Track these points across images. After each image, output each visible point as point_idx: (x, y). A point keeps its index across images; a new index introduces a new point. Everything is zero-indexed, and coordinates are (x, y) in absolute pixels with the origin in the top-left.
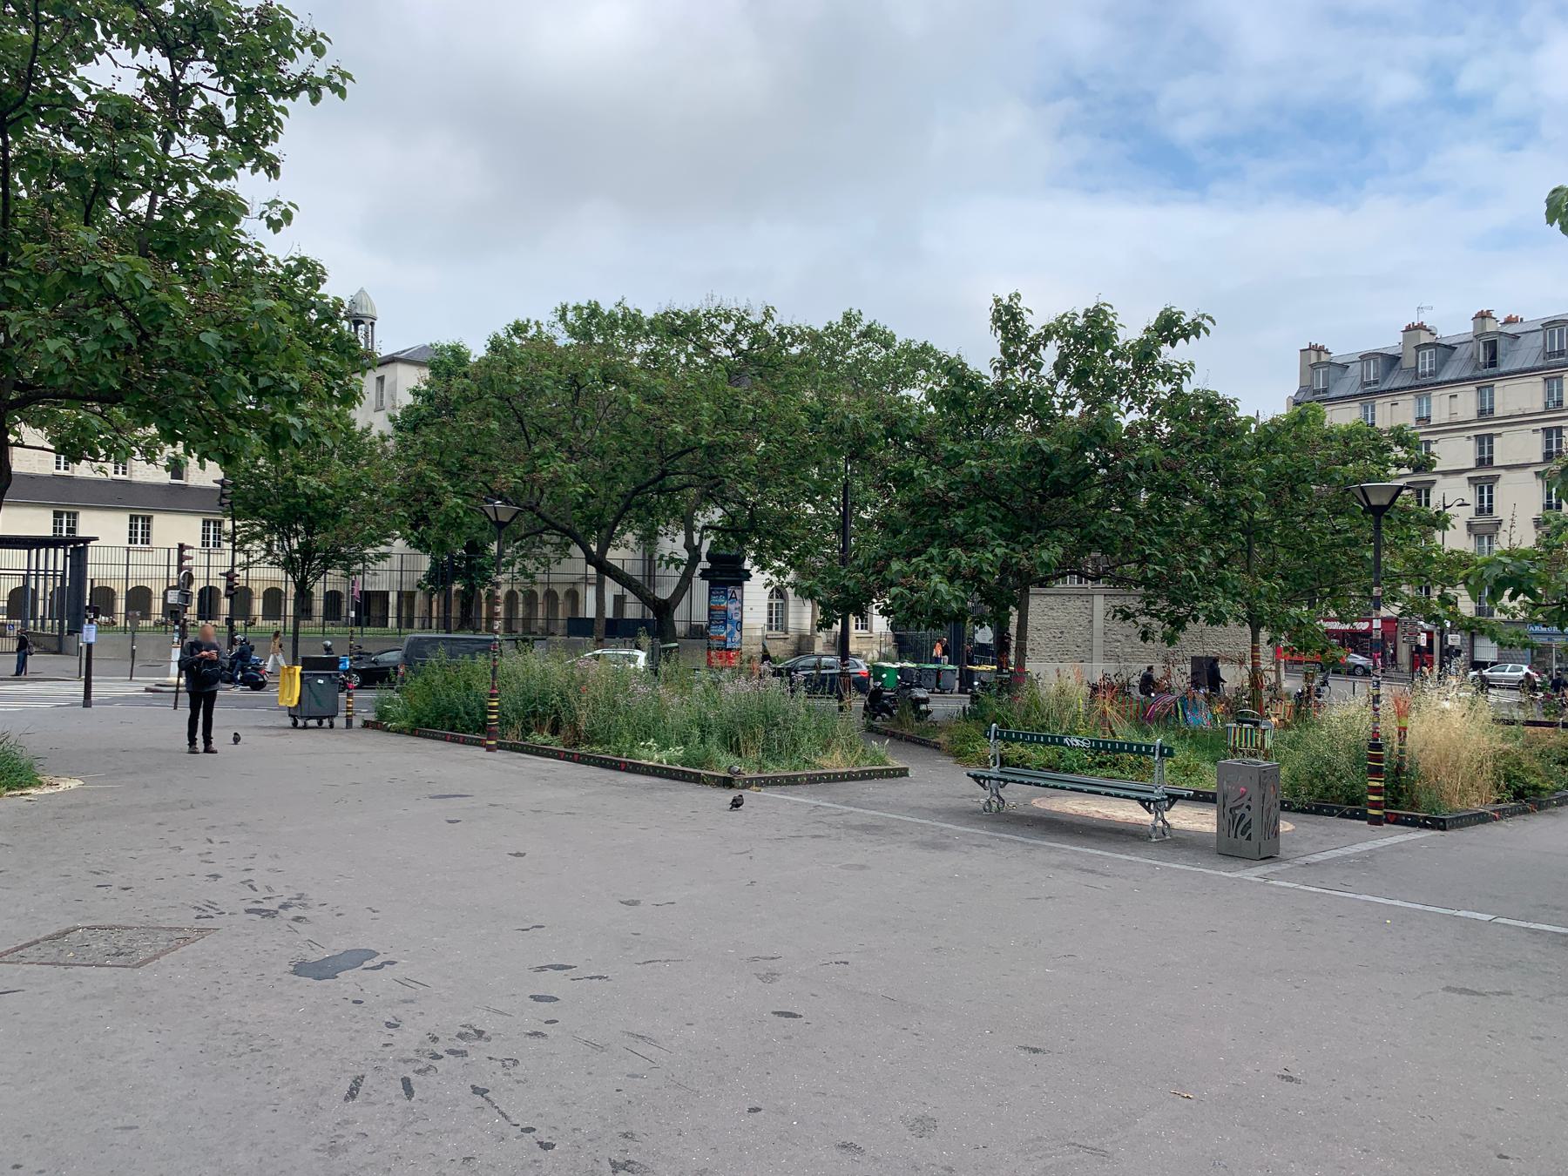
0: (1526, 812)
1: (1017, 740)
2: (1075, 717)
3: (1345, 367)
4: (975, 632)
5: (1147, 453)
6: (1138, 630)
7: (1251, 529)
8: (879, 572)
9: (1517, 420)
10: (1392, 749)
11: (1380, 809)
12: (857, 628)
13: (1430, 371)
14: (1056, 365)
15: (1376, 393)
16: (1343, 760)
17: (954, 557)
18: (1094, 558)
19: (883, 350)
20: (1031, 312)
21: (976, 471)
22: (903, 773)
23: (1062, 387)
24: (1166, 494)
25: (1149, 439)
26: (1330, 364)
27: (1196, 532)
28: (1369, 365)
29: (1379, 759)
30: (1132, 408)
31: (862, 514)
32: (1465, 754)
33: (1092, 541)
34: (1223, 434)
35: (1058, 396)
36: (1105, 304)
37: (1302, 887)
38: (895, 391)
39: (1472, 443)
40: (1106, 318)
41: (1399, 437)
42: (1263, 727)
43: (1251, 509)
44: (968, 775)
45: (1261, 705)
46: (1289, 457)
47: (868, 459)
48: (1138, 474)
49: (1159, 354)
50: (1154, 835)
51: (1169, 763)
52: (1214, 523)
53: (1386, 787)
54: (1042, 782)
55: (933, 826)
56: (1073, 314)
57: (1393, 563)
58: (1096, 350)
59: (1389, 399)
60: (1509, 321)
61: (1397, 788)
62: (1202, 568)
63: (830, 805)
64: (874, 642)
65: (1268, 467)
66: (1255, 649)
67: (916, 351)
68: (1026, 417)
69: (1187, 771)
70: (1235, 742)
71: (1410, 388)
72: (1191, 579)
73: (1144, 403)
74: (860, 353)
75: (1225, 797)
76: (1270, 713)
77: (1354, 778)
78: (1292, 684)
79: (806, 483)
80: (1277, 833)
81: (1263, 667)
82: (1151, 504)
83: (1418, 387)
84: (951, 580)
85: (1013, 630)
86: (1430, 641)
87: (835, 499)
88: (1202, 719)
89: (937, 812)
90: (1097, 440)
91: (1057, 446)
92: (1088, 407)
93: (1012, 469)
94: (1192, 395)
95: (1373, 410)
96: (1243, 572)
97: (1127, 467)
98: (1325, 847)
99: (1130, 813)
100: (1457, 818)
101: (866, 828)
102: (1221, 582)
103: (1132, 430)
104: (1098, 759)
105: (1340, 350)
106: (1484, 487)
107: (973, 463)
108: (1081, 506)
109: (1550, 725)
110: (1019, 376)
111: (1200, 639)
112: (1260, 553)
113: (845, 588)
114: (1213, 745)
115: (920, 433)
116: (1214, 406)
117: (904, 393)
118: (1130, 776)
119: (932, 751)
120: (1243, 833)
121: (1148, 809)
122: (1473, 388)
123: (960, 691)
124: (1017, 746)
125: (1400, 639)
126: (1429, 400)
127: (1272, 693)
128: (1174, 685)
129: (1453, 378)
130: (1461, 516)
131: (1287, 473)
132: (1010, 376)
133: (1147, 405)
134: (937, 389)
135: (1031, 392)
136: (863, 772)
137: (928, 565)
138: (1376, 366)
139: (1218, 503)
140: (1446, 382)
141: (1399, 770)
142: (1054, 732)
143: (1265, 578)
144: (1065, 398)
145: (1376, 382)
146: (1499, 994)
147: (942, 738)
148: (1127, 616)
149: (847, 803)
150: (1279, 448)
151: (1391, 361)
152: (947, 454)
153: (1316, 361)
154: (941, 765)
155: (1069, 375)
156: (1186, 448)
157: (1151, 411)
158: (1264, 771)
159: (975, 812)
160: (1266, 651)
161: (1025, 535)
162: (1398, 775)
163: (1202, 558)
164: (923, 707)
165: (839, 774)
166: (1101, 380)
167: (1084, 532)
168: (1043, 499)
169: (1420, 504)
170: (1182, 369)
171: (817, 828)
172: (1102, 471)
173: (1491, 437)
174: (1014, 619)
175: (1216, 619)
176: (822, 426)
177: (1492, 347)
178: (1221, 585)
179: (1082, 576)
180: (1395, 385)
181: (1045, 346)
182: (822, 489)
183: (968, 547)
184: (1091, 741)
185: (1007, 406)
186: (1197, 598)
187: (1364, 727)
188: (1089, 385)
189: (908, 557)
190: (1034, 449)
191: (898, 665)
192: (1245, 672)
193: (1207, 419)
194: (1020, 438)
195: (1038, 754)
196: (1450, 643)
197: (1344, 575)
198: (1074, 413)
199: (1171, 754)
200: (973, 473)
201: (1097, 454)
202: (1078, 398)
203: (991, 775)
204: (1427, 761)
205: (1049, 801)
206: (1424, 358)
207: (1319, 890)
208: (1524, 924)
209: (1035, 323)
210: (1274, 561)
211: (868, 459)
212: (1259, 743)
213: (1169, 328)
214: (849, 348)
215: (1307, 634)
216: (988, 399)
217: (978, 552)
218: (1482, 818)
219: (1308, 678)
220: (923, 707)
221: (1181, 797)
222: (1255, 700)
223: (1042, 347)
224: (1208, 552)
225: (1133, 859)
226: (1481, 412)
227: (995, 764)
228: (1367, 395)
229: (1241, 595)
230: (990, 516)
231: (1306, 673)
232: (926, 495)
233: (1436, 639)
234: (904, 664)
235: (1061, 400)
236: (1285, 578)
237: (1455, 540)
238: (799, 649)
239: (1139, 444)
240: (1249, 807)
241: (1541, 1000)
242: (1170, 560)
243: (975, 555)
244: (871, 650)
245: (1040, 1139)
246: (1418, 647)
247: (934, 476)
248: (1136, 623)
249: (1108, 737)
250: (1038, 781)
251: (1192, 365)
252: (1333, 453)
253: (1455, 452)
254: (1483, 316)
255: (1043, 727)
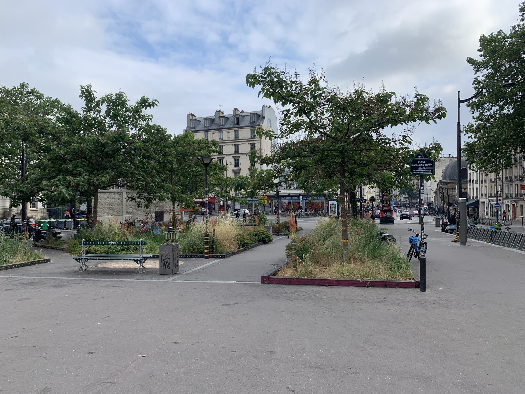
0: (245, 250)
1: (92, 244)
2: (115, 234)
3: (200, 121)
4: (80, 207)
5: (138, 144)
6: (136, 204)
7: (172, 170)
8: (37, 185)
9: (244, 140)
10: (211, 236)
11: (208, 254)
12: (31, 207)
13: (223, 125)
14: (106, 112)
15: (208, 130)
16: (198, 241)
17: (68, 179)
18: (120, 180)
19: (39, 100)
20: (96, 92)
21: (76, 148)
22: (48, 261)
23: (108, 120)
24: (145, 158)
25: (139, 140)
26: (195, 120)
27: (154, 171)
28: (206, 121)
29: (207, 239)
30: (133, 129)
31: (31, 163)
32: (230, 236)
33: (120, 174)
34: (162, 140)
35: (107, 123)
36: (123, 92)
37: (185, 281)
38: (44, 116)
39: (233, 146)
40: (123, 97)
41: (213, 143)
42: (176, 232)
43: (172, 164)
44: (73, 259)
45: (176, 226)
46: (183, 148)
47: (33, 141)
48: (135, 151)
49: (141, 111)
50: (139, 271)
51: (145, 247)
52: (160, 168)
53: (210, 247)
54: (101, 258)
55: (59, 279)
56: (112, 94)
57: (211, 180)
58: (120, 108)
59: (212, 132)
60: (242, 112)
61: (213, 247)
62: (156, 183)
63: (15, 277)
64: (38, 212)
65: (176, 151)
66: (174, 208)
67: (53, 101)
68: (95, 130)
69: (151, 249)
70: (167, 238)
71: (217, 129)
72: (153, 187)
73: (137, 127)
74: (28, 100)
75: (162, 256)
76: (179, 228)
77: (201, 246)
78: (186, 219)
79: (4, 150)
80: (178, 265)
81: (176, 213)
82: (140, 162)
83: (219, 129)
84: (67, 187)
85: (93, 205)
86: (224, 204)
87: (19, 156)
88: (157, 232)
89: (60, 274)
90: (120, 140)
91: (106, 141)
92: (118, 127)
93: (90, 147)
94: (152, 126)
95: (208, 135)
96: (169, 184)
97: (131, 149)
98: (192, 268)
99: (132, 265)
100: (229, 254)
101: (30, 284)
102: (163, 187)
103: (133, 136)
104: (122, 248)
105: (199, 115)
106: (236, 159)
107: (75, 145)
108: (117, 161)
109: (251, 225)
110: (93, 115)
111: (156, 206)
112: (175, 178)
113: (22, 192)
114: (159, 239)
115: (54, 133)
116: (160, 130)
117: (48, 117)
118: (133, 253)
119: (62, 251)
120: (167, 267)
121: (137, 263)
122: (233, 130)
123: (74, 229)
124: (93, 246)
125: (216, 203)
126: (222, 133)
127: (179, 222)
128: (149, 221)
129: (228, 127)
130: (230, 168)
131: (182, 153)
132: (89, 114)
133: (138, 128)
134: (60, 117)
135: (97, 121)
136: (31, 263)
137: (58, 182)
138: (208, 121)
139: (161, 162)
140: (227, 128)
141: (213, 242)
142: (107, 240)
143: (176, 186)
144: (109, 123)
145: (208, 127)
146: (235, 304)
147: (65, 246)
148: (133, 199)
149: (23, 275)
150: (180, 145)
151: (212, 121)
152: (65, 141)
153: (191, 118)
154: (64, 256)
155: (111, 116)
156: (151, 144)
157: (139, 130)
158: (174, 246)
159: (76, 272)
160: (177, 209)
161: (96, 171)
162: (213, 243)
163: (156, 180)
164: (58, 235)
165: (20, 264)
166: (122, 118)
167: (118, 170)
168: (102, 159)
169: (220, 163)
170: (149, 117)
171: (8, 287)
172: (123, 150)
173: (238, 145)
174: (93, 201)
175: (161, 199)
176: (11, 127)
177: (238, 119)
178: (163, 188)
179: (119, 186)
180: (214, 128)
181: (102, 105)
182: (12, 152)
183: (74, 175)
184: (118, 242)
185: (88, 125)
186: (155, 192)
187: (203, 231)
188: (118, 120)
189: (50, 179)
190: (98, 141)
191: (49, 220)
192: (171, 216)
193: (157, 134)
194: (93, 137)
195: (101, 249)
196: (228, 204)
197: (199, 185)
198: (113, 129)
199: (145, 244)
200: (75, 149)
201: (121, 144)
202: (114, 124)
203: (82, 258)
204: (220, 238)
205: (104, 264)
206: (221, 121)
207: (190, 281)
208: (242, 283)
209: (98, 96)
210: (179, 181)
211: (33, 141)
212: (175, 238)
213: (144, 103)
214: (23, 97)
215: (189, 203)
216: (80, 122)
217: (78, 178)
218: (234, 254)
219: (190, 217)
220: (58, 235)
221: (148, 258)
222: (174, 225)
223: (100, 105)
224: (158, 177)
225: (132, 280)
226: (236, 138)
227: (84, 253)
228: (206, 130)
229: (169, 191)
230: (83, 164)
231: (189, 215)
232: (56, 156)
233: (225, 203)
234: (51, 220)
235: (108, 124)
236: (182, 186)
237: (229, 174)
238: (4, 216)
239: (135, 141)
240: (169, 258)
241: (245, 303)
242: (146, 180)
243: (77, 178)
244: (37, 215)
245: (91, 384)
246: (220, 205)
247: (60, 149)
248: (136, 201)
249: (126, 240)
250: (99, 258)
251: (152, 116)
252: (195, 147)
253: (228, 149)
254: (236, 110)
255: (103, 239)
